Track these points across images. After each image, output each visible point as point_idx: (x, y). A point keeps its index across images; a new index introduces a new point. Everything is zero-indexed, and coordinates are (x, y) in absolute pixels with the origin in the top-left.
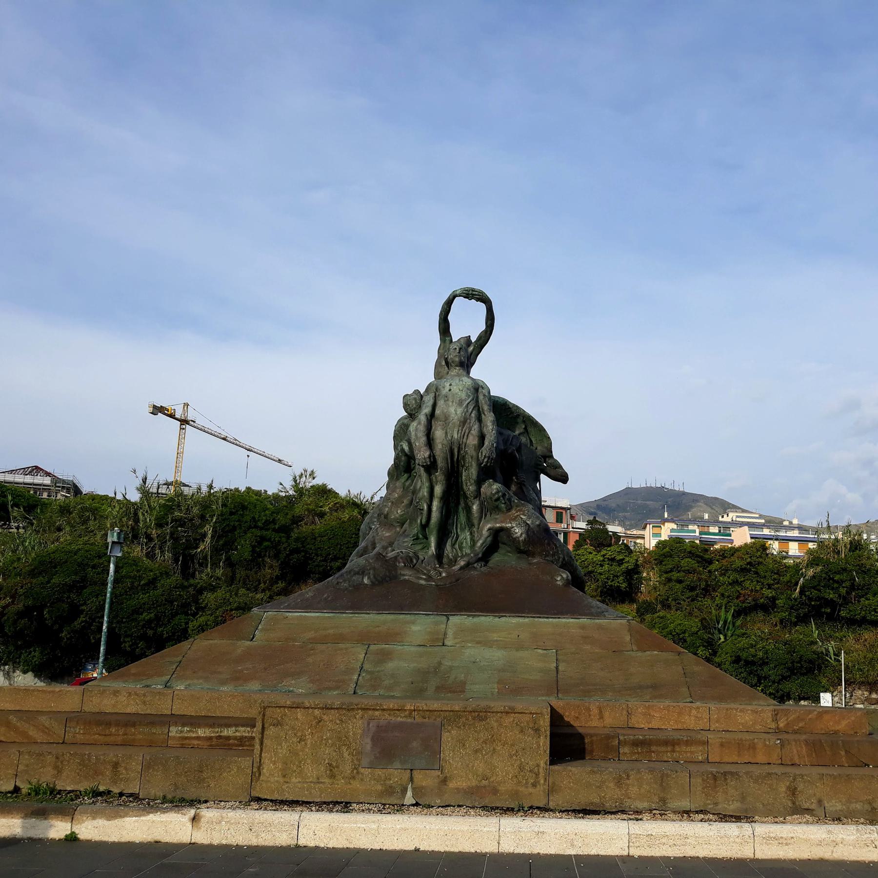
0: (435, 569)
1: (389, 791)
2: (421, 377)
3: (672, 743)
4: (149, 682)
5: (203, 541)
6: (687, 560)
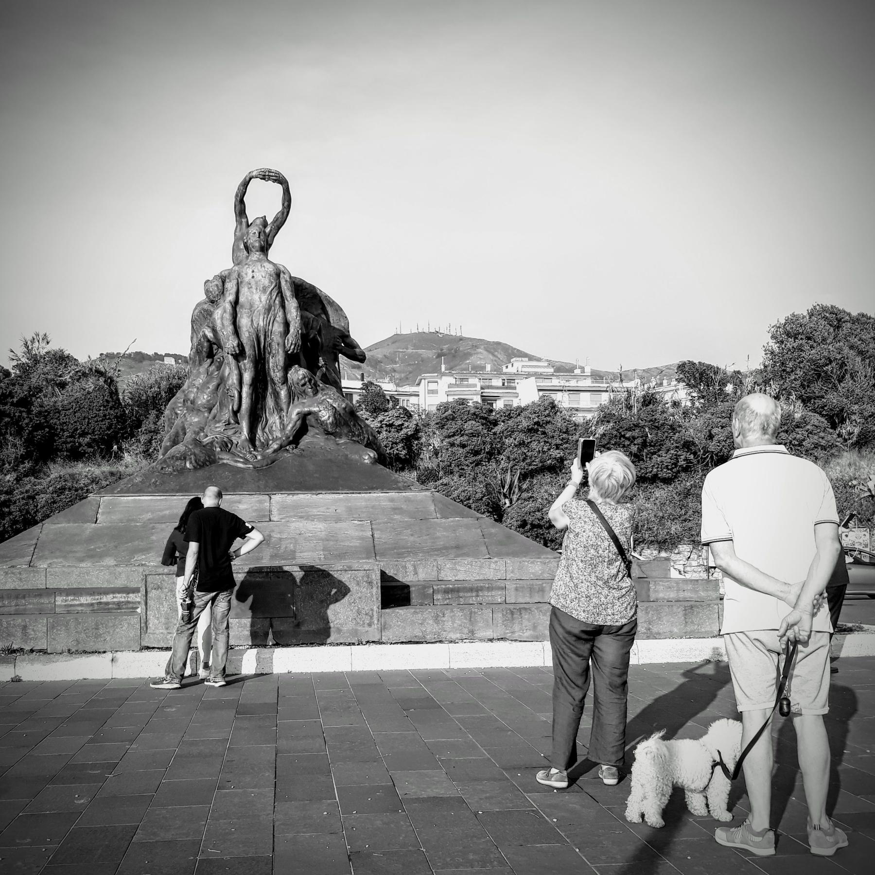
0: (250, 453)
2: (222, 261)
3: (476, 590)
4: (13, 563)
6: (470, 422)
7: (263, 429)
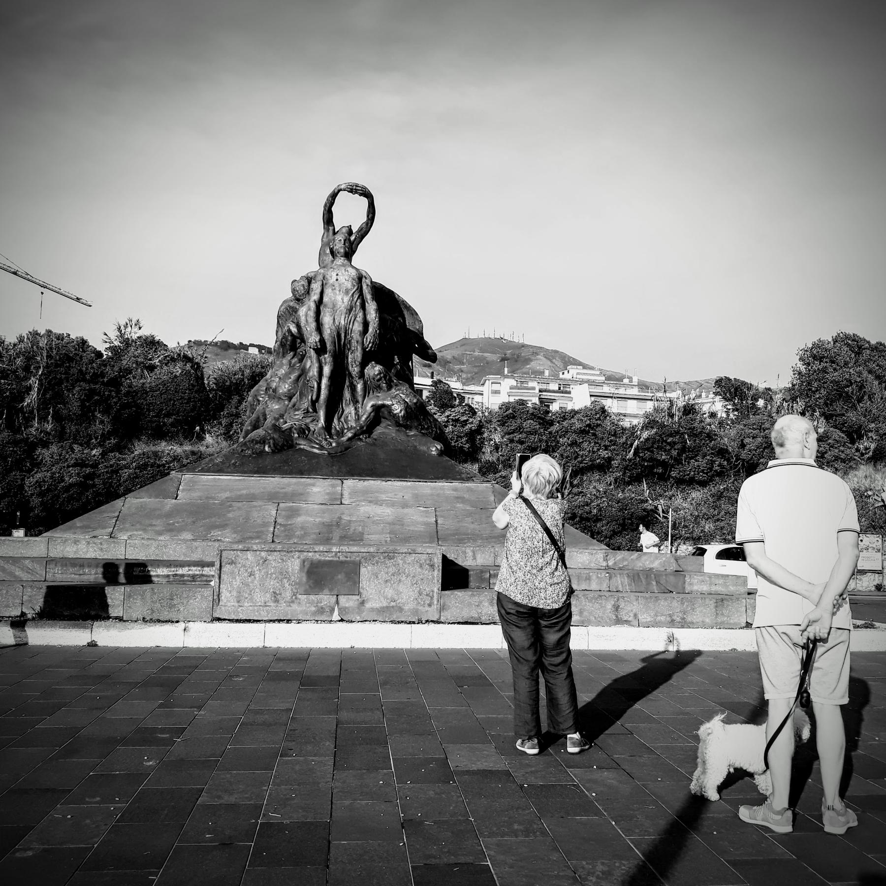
0: (326, 439)
1: (321, 611)
5: (29, 394)
6: (529, 421)
7: (339, 419)
